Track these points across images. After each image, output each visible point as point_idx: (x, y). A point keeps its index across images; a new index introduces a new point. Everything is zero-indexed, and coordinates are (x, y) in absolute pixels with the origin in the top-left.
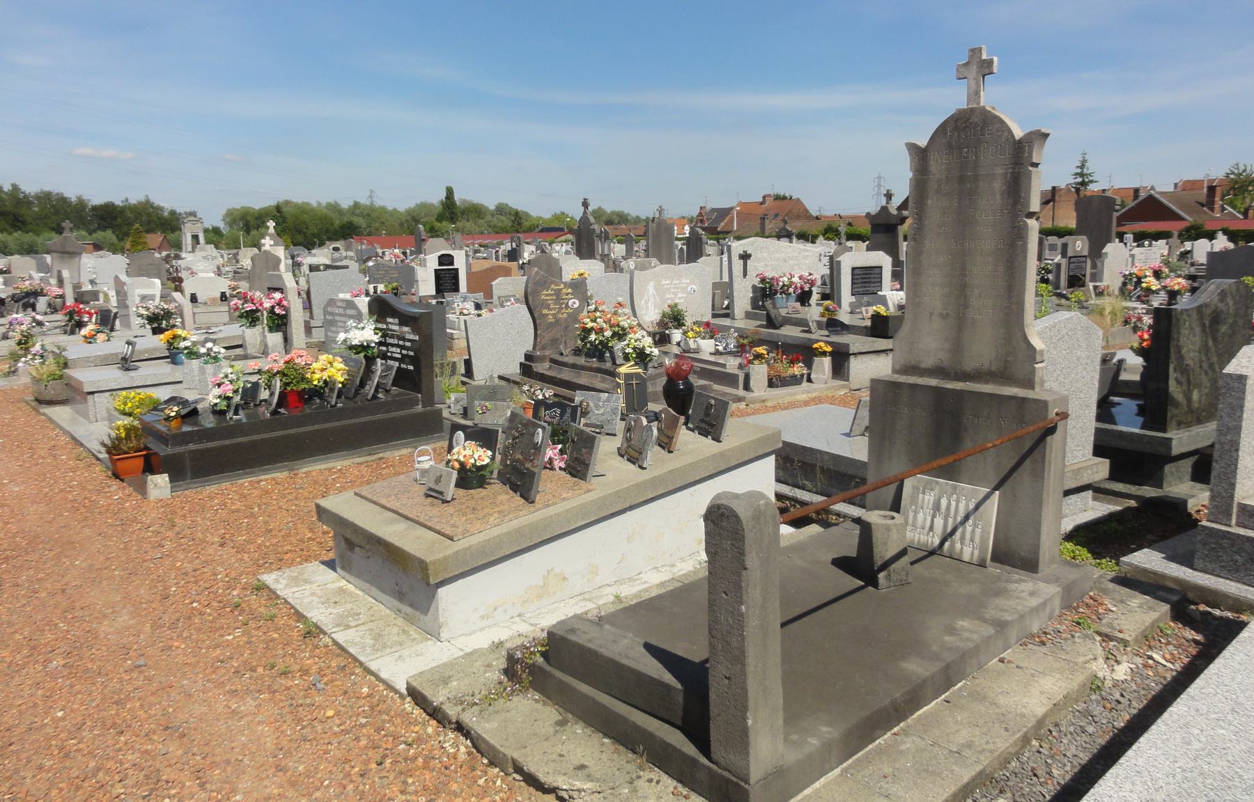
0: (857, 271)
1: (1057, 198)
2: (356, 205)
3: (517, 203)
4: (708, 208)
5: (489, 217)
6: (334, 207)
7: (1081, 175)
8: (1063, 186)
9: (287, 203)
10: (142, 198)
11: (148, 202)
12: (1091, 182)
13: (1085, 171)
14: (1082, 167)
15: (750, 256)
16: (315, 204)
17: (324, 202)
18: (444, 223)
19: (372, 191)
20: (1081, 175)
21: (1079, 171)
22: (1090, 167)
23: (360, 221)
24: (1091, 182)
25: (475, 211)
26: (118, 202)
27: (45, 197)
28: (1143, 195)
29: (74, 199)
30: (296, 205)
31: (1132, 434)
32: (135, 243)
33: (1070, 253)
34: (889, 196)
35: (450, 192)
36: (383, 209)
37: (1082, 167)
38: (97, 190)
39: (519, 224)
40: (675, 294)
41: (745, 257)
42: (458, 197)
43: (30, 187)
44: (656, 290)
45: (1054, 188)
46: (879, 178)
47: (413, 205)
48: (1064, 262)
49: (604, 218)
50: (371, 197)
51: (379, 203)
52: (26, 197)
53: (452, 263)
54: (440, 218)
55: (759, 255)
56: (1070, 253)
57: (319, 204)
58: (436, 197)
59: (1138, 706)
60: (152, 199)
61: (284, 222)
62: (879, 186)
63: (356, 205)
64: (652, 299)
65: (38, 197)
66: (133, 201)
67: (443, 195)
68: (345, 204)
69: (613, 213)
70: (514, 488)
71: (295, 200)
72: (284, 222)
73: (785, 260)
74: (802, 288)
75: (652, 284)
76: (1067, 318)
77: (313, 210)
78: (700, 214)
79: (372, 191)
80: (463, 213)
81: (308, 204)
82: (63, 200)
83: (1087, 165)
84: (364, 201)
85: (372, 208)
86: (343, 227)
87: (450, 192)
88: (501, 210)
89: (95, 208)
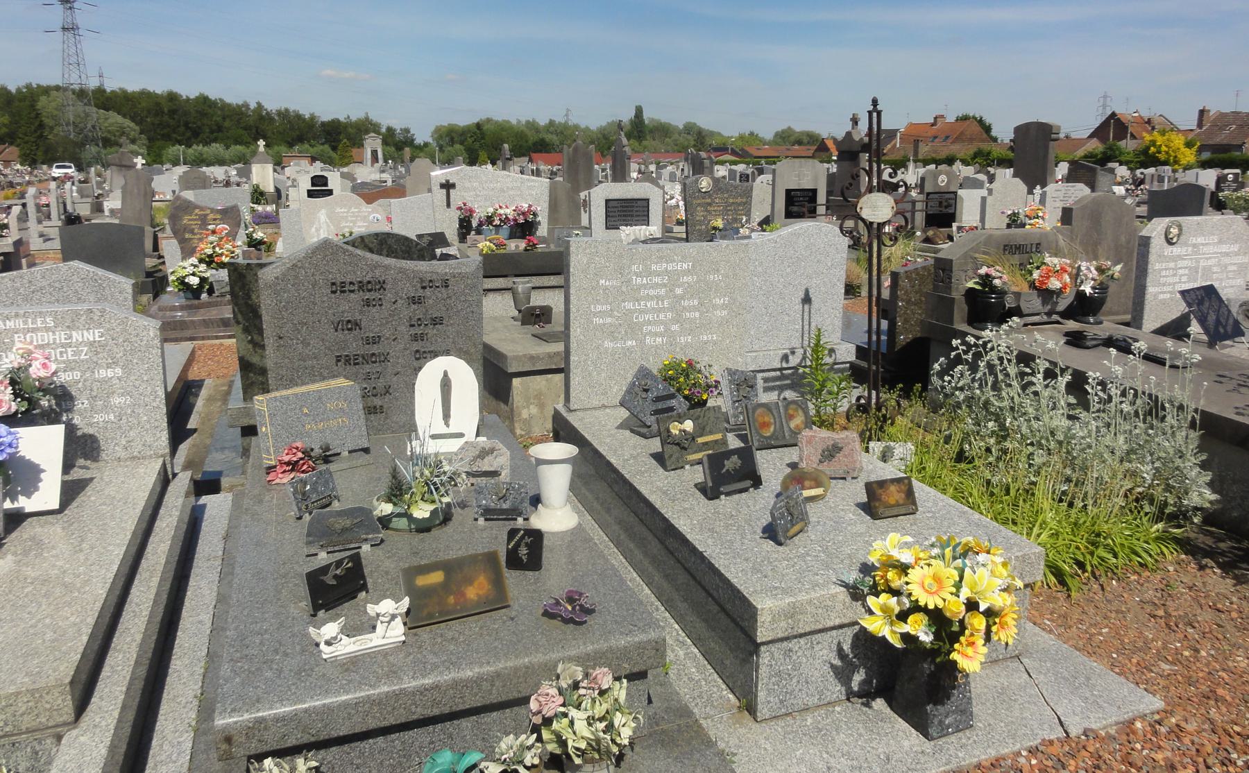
0: (611, 204)
2: (552, 123)
3: (706, 122)
6: (532, 125)
9: (489, 120)
10: (361, 115)
11: (367, 118)
15: (453, 186)
16: (514, 122)
17: (523, 120)
23: (549, 137)
25: (663, 131)
26: (342, 119)
27: (284, 114)
30: (497, 122)
32: (343, 157)
33: (928, 188)
34: (855, 121)
35: (639, 111)
36: (576, 127)
38: (325, 106)
39: (702, 143)
40: (354, 222)
41: (448, 186)
42: (647, 116)
43: (272, 106)
44: (330, 218)
46: (1105, 97)
47: (604, 124)
48: (921, 197)
49: (792, 139)
51: (574, 120)
52: (268, 113)
53: (326, 185)
55: (467, 185)
56: (928, 188)
57: (519, 122)
58: (627, 115)
59: (446, 710)
61: (483, 138)
62: (1104, 106)
63: (552, 123)
64: (324, 226)
65: (279, 113)
66: (354, 118)
67: (632, 114)
68: (542, 121)
69: (802, 133)
71: (495, 118)
72: (483, 138)
73: (502, 190)
74: (515, 220)
75: (323, 211)
77: (511, 127)
80: (651, 131)
81: (508, 122)
82: (299, 117)
84: (559, 119)
85: (565, 126)
86: (535, 144)
87: (639, 111)
88: (690, 129)
89: (323, 124)
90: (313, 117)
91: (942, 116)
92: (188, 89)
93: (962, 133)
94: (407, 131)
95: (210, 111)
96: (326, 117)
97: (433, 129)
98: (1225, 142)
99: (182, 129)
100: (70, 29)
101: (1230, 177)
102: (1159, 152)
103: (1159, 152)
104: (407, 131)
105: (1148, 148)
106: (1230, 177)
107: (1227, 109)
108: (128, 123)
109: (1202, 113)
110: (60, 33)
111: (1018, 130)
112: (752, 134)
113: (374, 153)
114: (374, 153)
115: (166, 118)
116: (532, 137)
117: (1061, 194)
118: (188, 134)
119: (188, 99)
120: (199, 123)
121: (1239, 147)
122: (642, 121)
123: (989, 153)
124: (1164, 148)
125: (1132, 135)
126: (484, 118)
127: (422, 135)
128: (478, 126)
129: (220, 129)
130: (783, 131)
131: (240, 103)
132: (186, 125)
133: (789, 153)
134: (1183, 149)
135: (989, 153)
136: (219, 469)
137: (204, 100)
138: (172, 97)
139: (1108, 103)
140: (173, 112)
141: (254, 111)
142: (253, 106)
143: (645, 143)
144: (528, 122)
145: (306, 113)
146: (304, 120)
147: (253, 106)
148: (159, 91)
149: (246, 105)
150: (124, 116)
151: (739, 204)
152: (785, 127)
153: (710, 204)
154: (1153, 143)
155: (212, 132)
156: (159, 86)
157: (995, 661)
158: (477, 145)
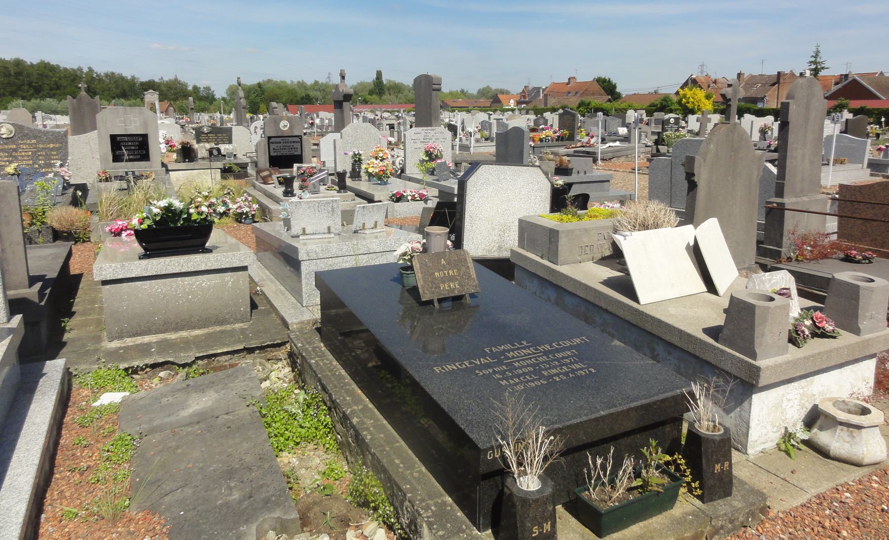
1: (781, 81)
2: (316, 83)
4: (531, 87)
5: (406, 92)
6: (302, 85)
7: (815, 63)
8: (787, 72)
9: (269, 81)
10: (172, 77)
11: (176, 80)
12: (823, 68)
13: (818, 60)
14: (816, 56)
16: (289, 82)
18: (374, 96)
19: (329, 74)
20: (815, 63)
21: (813, 59)
22: (822, 58)
23: (312, 94)
24: (823, 68)
25: (397, 89)
26: (157, 80)
27: (111, 76)
28: (850, 79)
29: (129, 78)
31: (196, 336)
35: (379, 74)
37: (816, 56)
45: (779, 73)
46: (702, 66)
50: (329, 77)
54: (371, 93)
57: (292, 82)
58: (370, 78)
60: (179, 79)
61: (263, 94)
63: (316, 83)
65: (107, 75)
66: (166, 79)
68: (309, 81)
70: (351, 317)
72: (263, 94)
76: (303, 198)
78: (523, 92)
79: (329, 74)
80: (389, 89)
81: (284, 82)
82: (122, 78)
83: (820, 55)
86: (302, 98)
87: (379, 74)
90: (133, 78)
91: (574, 78)
92: (32, 57)
93: (586, 90)
95: (51, 74)
97: (227, 87)
98: (753, 96)
99: (26, 87)
101: (672, 121)
102: (688, 103)
103: (688, 103)
105: (681, 100)
106: (672, 121)
107: (756, 72)
109: (739, 75)
111: (415, 80)
112: (462, 91)
115: (12, 79)
116: (301, 93)
117: (421, 137)
118: (32, 91)
119: (32, 65)
120: (40, 83)
121: (762, 99)
122: (381, 82)
123: (589, 104)
124: (691, 100)
126: (265, 79)
127: (220, 93)
128: (259, 85)
129: (58, 87)
130: (484, 89)
131: (75, 67)
132: (30, 84)
133: (476, 104)
134: (704, 100)
135: (589, 104)
138: (18, 63)
139: (705, 69)
140: (18, 74)
141: (87, 74)
142: (85, 70)
143: (384, 97)
144: (299, 82)
146: (127, 81)
147: (85, 70)
149: (80, 69)
151: (52, 149)
153: (15, 150)
154: (685, 96)
155: (51, 90)
157: (385, 377)
158: (258, 99)
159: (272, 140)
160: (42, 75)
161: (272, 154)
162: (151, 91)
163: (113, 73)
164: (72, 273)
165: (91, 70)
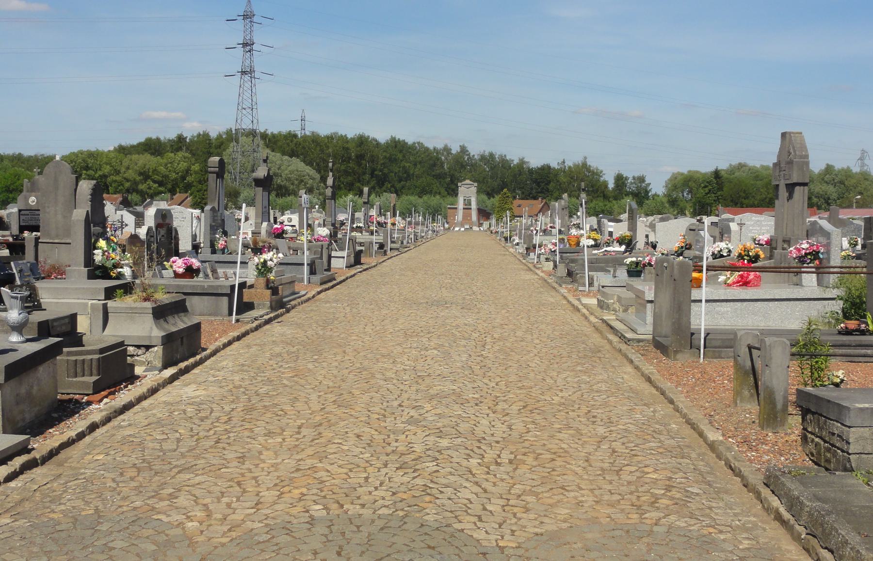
2: (829, 169)
9: (741, 166)
11: (584, 165)
19: (863, 152)
26: (554, 165)
50: (861, 159)
66: (569, 163)
72: (721, 188)
79: (863, 152)
82: (505, 163)
89: (531, 171)
92: (381, 132)
94: (642, 179)
95: (400, 156)
96: (535, 161)
100: (247, 72)
104: (642, 179)
108: (309, 170)
110: (237, 79)
113: (468, 203)
114: (468, 203)
125: (279, 169)
126: (735, 162)
127: (658, 187)
128: (717, 174)
129: (409, 177)
131: (440, 146)
136: (189, 310)
137: (396, 145)
138: (362, 141)
140: (360, 157)
145: (514, 157)
148: (350, 135)
149: (447, 149)
150: (309, 163)
152: (845, 167)
156: (350, 129)
159: (22, 212)
160: (392, 160)
161: (22, 224)
162: (468, 181)
163: (492, 155)
164: (78, 331)
165: (463, 150)
